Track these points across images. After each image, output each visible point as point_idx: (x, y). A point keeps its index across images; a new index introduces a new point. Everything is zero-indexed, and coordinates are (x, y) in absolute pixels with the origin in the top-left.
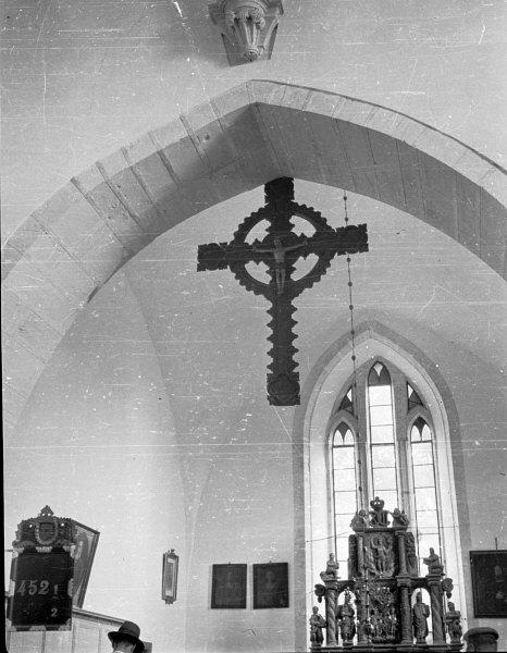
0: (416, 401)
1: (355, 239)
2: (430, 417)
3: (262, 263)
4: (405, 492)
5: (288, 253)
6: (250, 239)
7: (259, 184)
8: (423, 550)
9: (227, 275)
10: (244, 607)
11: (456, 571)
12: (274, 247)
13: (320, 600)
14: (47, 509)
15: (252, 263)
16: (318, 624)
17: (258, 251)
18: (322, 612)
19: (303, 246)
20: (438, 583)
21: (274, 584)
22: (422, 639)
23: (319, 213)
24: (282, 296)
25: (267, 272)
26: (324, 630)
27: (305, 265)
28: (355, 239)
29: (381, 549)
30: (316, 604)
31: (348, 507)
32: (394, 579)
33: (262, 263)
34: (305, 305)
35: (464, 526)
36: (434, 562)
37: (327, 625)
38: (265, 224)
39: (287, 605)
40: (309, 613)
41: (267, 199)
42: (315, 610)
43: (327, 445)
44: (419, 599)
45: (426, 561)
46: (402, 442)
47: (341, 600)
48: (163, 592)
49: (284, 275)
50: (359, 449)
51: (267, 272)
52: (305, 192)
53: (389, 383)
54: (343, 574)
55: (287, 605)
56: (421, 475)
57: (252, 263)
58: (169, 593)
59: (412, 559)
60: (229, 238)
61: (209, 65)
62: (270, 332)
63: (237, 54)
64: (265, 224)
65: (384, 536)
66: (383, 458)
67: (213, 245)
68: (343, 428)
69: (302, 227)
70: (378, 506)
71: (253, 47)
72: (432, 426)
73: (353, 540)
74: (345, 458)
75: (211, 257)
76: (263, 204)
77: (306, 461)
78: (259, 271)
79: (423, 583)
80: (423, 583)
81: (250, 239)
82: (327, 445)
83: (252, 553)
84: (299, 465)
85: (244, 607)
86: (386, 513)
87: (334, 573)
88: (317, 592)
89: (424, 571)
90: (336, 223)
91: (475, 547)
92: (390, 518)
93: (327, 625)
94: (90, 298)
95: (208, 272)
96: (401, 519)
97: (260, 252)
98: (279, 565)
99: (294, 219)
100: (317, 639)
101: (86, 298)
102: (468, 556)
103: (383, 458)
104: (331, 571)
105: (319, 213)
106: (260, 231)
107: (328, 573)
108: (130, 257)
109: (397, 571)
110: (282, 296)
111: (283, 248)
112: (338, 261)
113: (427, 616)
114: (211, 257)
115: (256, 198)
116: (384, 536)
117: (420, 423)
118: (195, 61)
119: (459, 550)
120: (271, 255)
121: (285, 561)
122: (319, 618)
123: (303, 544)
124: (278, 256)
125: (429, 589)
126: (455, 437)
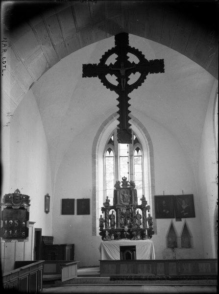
1: (158, 66)
2: (142, 147)
3: (113, 75)
4: (131, 173)
5: (126, 71)
6: (108, 63)
10: (78, 200)
11: (150, 202)
12: (120, 67)
13: (103, 213)
14: (18, 190)
15: (109, 75)
17: (112, 69)
18: (103, 217)
19: (133, 68)
20: (144, 207)
21: (84, 206)
23: (141, 52)
24: (123, 91)
25: (116, 80)
26: (104, 223)
27: (134, 78)
28: (158, 66)
29: (126, 195)
33: (113, 75)
34: (134, 96)
36: (143, 199)
37: (105, 221)
39: (89, 214)
41: (116, 43)
42: (101, 216)
43: (104, 156)
44: (138, 212)
45: (141, 200)
47: (110, 213)
48: (45, 209)
49: (125, 81)
50: (130, 158)
51: (116, 80)
52: (134, 41)
54: (111, 204)
55: (89, 214)
56: (137, 168)
57: (109, 75)
58: (47, 210)
60: (98, 62)
62: (118, 103)
65: (125, 190)
66: (124, 163)
67: (90, 65)
68: (110, 150)
69: (133, 59)
73: (115, 192)
74: (110, 162)
75: (89, 71)
76: (114, 46)
77: (96, 162)
78: (112, 79)
81: (108, 63)
82: (104, 156)
83: (76, 194)
84: (94, 163)
86: (127, 182)
87: (108, 203)
88: (102, 210)
89: (140, 203)
90: (150, 57)
91: (159, 193)
92: (128, 183)
93: (105, 221)
94: (30, 87)
95: (87, 78)
96: (132, 184)
97: (112, 70)
98: (86, 200)
99: (129, 54)
100: (101, 226)
101: (29, 87)
102: (154, 197)
103: (124, 163)
104: (107, 202)
105: (141, 52)
106: (112, 60)
107: (106, 203)
108: (50, 67)
110: (123, 91)
111: (123, 69)
112: (150, 77)
113: (141, 218)
114: (89, 71)
115: (110, 42)
116: (125, 190)
117: (138, 150)
119: (151, 195)
120: (119, 71)
122: (102, 219)
124: (123, 72)
125: (142, 209)
126: (152, 155)
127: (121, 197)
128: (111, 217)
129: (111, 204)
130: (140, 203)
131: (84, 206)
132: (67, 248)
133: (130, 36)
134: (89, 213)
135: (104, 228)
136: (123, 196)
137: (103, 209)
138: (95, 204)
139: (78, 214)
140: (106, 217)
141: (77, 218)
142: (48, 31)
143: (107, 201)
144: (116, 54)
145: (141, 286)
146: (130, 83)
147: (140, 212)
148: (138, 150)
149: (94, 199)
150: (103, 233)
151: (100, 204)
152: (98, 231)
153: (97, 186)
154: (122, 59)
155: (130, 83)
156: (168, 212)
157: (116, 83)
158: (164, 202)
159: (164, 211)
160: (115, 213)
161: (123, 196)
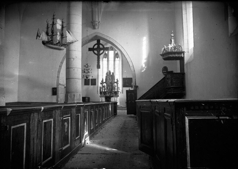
0: (117, 54)
6: (95, 47)
7: (96, 40)
8: (116, 79)
9: (92, 52)
16: (100, 88)
22: (115, 90)
24: (99, 55)
30: (100, 85)
31: (105, 71)
32: (111, 82)
35: (122, 74)
37: (102, 88)
38: (95, 51)
40: (99, 86)
46: (114, 60)
47: (104, 85)
52: (101, 42)
53: (113, 50)
54: (104, 81)
59: (114, 79)
61: (91, 29)
63: (94, 28)
64: (95, 51)
65: (110, 76)
68: (105, 58)
70: (110, 72)
71: (96, 28)
72: (119, 58)
75: (90, 49)
79: (116, 83)
80: (116, 83)
85: (89, 85)
89: (116, 81)
91: (125, 77)
100: (100, 90)
104: (103, 80)
106: (96, 47)
109: (112, 81)
111: (99, 49)
114: (90, 49)
115: (96, 42)
116: (110, 76)
117: (117, 57)
118: (101, 131)
121: (95, 78)
123: (98, 76)
127: (108, 78)
128: (104, 87)
129: (104, 81)
130: (116, 81)
131: (94, 82)
132: (86, 98)
133: (101, 40)
134: (96, 85)
135: (101, 91)
136: (109, 78)
137: (101, 83)
138: (98, 81)
139: (91, 85)
140: (102, 87)
141: (91, 87)
142: (71, 68)
143: (103, 80)
144: (100, 42)
145: (172, 124)
146: (100, 53)
147: (116, 84)
148: (117, 57)
149: (98, 79)
150: (101, 93)
151: (100, 81)
152: (99, 92)
153: (99, 74)
154: (98, 47)
155: (100, 53)
156: (128, 85)
157: (97, 53)
158: (127, 81)
159: (127, 84)
160: (106, 85)
161: (109, 78)
